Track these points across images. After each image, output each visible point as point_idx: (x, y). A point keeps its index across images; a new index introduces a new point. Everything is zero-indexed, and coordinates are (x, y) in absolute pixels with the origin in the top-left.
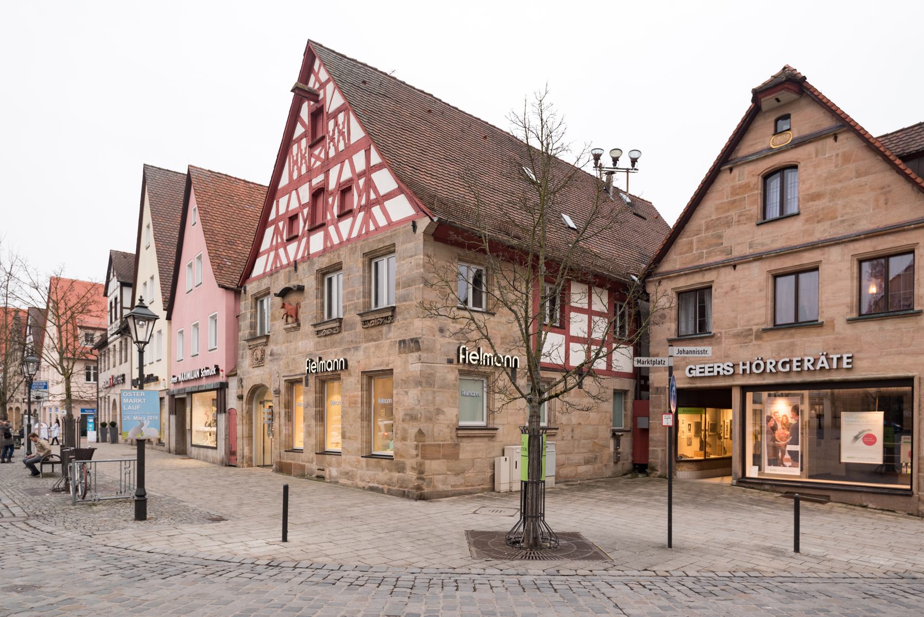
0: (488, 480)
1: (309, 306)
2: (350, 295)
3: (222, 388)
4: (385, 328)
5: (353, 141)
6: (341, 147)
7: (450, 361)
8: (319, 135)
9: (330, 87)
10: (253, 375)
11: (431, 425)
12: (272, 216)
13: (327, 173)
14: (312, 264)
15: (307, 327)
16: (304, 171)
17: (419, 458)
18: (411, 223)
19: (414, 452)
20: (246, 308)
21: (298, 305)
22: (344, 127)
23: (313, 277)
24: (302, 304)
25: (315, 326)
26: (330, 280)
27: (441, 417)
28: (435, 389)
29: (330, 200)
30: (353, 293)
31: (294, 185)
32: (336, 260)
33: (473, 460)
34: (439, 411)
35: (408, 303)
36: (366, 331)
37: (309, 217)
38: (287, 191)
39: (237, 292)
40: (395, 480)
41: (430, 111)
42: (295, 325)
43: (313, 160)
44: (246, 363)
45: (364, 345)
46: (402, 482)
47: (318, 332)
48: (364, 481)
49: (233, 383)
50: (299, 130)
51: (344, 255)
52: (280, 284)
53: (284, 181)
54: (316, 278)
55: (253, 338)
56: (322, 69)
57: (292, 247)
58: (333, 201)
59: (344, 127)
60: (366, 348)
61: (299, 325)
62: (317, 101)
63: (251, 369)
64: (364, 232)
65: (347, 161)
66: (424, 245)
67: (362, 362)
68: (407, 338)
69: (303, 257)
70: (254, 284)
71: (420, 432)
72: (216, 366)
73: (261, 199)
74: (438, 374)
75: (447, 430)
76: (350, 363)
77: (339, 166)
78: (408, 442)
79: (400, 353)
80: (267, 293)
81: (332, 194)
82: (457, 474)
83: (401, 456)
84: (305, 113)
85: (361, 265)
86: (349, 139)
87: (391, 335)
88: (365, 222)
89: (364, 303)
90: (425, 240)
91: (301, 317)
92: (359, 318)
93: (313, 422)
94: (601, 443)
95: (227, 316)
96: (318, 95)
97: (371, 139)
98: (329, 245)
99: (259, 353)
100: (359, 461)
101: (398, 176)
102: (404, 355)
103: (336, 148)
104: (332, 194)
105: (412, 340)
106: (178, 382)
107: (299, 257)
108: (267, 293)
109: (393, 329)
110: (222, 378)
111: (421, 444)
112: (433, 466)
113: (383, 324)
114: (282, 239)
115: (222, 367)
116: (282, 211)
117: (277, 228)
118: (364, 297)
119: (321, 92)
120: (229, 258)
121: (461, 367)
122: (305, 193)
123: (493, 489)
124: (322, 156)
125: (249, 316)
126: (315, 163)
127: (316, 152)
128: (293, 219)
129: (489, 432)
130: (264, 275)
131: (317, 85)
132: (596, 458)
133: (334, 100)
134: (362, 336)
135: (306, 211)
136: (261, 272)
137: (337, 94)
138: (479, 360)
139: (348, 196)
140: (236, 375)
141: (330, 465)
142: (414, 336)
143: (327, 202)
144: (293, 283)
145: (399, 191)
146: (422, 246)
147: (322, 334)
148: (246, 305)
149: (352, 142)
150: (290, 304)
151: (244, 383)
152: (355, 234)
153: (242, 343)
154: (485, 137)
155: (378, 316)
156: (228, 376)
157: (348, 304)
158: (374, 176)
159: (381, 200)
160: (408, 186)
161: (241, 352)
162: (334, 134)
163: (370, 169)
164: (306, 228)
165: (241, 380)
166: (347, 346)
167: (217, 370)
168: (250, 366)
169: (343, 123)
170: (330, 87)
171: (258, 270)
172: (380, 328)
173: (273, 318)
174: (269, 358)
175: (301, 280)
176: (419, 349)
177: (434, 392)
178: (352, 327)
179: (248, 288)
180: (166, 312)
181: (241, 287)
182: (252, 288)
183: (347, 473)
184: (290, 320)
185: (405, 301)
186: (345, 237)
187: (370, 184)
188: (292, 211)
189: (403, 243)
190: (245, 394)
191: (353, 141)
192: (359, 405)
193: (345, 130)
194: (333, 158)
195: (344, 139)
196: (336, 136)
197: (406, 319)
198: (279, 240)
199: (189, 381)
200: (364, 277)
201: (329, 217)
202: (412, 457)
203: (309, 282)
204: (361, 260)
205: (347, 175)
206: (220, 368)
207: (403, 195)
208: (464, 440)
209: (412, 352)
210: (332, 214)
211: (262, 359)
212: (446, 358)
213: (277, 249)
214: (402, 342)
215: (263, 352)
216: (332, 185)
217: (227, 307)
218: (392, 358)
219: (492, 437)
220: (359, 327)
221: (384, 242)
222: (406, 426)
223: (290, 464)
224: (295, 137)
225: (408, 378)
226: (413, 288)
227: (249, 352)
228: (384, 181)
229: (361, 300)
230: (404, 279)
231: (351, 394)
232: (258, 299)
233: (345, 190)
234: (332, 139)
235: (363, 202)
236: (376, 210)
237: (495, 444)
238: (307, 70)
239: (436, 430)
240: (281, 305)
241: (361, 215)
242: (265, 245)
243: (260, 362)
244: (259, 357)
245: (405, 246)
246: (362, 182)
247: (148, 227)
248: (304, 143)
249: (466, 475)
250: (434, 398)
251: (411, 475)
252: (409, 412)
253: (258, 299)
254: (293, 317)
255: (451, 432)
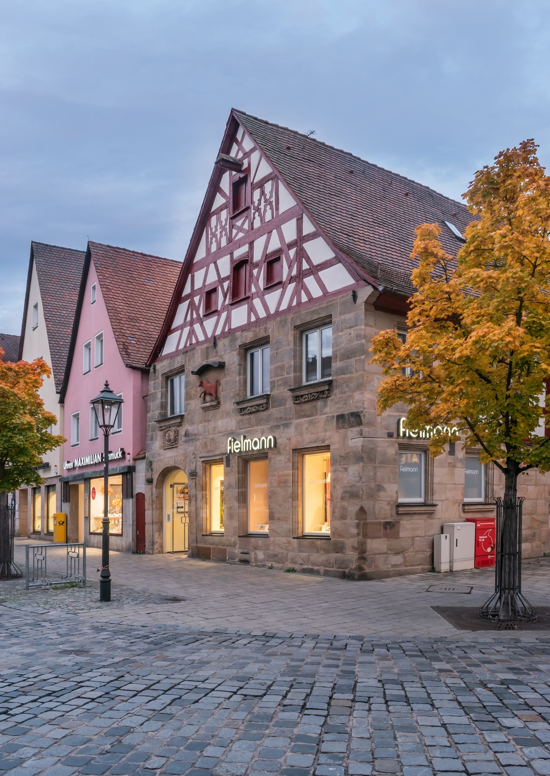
0: (428, 560)
1: (229, 384)
2: (278, 371)
3: (128, 473)
4: (319, 403)
5: (282, 210)
6: (268, 217)
7: (390, 435)
8: (243, 207)
9: (255, 156)
10: (165, 457)
11: (372, 502)
12: (187, 290)
13: (251, 244)
14: (234, 340)
15: (228, 405)
16: (224, 243)
17: (361, 537)
18: (351, 293)
19: (354, 531)
20: (155, 388)
21: (218, 383)
22: (271, 196)
23: (235, 353)
24: (223, 382)
25: (238, 403)
26: (252, 355)
27: (382, 494)
28: (377, 465)
29: (255, 271)
30: (282, 368)
31: (212, 259)
32: (262, 334)
33: (413, 538)
34: (380, 488)
35: (347, 376)
36: (298, 407)
37: (231, 291)
38: (204, 263)
39: (145, 372)
40: (332, 560)
41: (351, 172)
42: (214, 403)
43: (234, 231)
44: (156, 444)
45: (296, 422)
46: (342, 563)
47: (241, 410)
48: (295, 563)
49: (141, 467)
50: (219, 201)
51: (272, 329)
52: (198, 361)
53: (201, 254)
54: (239, 354)
55: (163, 419)
56: (247, 137)
57: (210, 323)
58: (259, 273)
59: (271, 196)
60: (298, 424)
61: (219, 403)
62: (239, 171)
63: (162, 451)
64: (294, 303)
65: (275, 232)
66: (366, 315)
67: (294, 440)
68: (346, 412)
69: (223, 332)
70: (166, 363)
71: (362, 510)
72: (122, 450)
73: (175, 275)
74: (379, 449)
75: (387, 508)
76: (279, 441)
77: (265, 237)
78: (348, 521)
79: (338, 428)
80: (181, 371)
81: (257, 265)
82: (397, 553)
83: (340, 536)
84: (226, 184)
85: (291, 339)
86: (277, 209)
87: (327, 410)
88: (297, 293)
89: (295, 377)
90: (366, 310)
91: (222, 394)
92: (289, 394)
93: (236, 504)
94: (539, 518)
95: (134, 396)
96: (241, 165)
97: (305, 206)
98: (253, 319)
99: (172, 434)
100: (289, 543)
101: (334, 245)
102: (342, 431)
103: (262, 219)
104: (257, 265)
105: (352, 414)
106: (74, 468)
107: (218, 332)
108: (181, 371)
109: (329, 403)
110: (129, 461)
111: (362, 522)
112: (375, 545)
113: (318, 399)
114: (198, 315)
115: (129, 449)
116: (198, 285)
117: (192, 304)
118: (295, 371)
119: (246, 162)
120: (133, 336)
121: (400, 441)
122: (225, 266)
123: (433, 570)
124: (246, 226)
125: (159, 395)
126: (237, 234)
127: (239, 223)
128: (210, 294)
129: (428, 508)
130: (177, 352)
131: (240, 155)
132: (534, 535)
133: (260, 168)
134: (293, 412)
135: (226, 285)
136: (173, 349)
137: (264, 162)
138: (240, 448)
139: (276, 266)
140: (144, 458)
141: (256, 548)
142: (354, 410)
143: (251, 275)
144: (213, 360)
145: (337, 260)
146: (363, 316)
147: (246, 411)
148: (155, 385)
149: (281, 212)
150: (209, 382)
151: (154, 466)
152: (284, 306)
153: (152, 423)
154: (407, 195)
155: (311, 391)
156: (135, 460)
157: (276, 379)
158: (308, 246)
159: (314, 270)
160: (345, 254)
161: (149, 434)
162: (259, 204)
163: (301, 239)
164: (227, 302)
165: (150, 464)
166: (275, 424)
167: (123, 453)
168: (161, 447)
169: (271, 192)
170: (255, 156)
171: (170, 347)
172: (314, 403)
173: (188, 397)
174: (184, 438)
175: (221, 357)
176: (360, 423)
177: (375, 468)
178: (281, 402)
179: (157, 367)
180: (59, 395)
181: (150, 366)
182: (162, 367)
183: (275, 556)
184: (208, 398)
185: (344, 374)
186: (272, 311)
187: (302, 254)
188: (210, 285)
189: (341, 314)
190: (155, 477)
191: (282, 210)
192: (290, 484)
193: (273, 199)
194: (259, 229)
195: (271, 208)
196: (262, 207)
197: (345, 393)
198: (195, 316)
199: (87, 466)
200: (295, 351)
201: (253, 290)
202: (353, 536)
203: (231, 358)
204: (291, 333)
205: (275, 244)
206: (127, 451)
207: (340, 265)
208: (405, 517)
209: (352, 427)
210: (257, 287)
211: (176, 440)
212: (386, 431)
213: (192, 324)
214: (341, 417)
215: (177, 433)
216: (257, 256)
217: (134, 388)
218: (328, 434)
219: (431, 514)
220: (290, 403)
221: (319, 314)
222: (345, 504)
223: (209, 549)
224: (213, 209)
225: (348, 454)
226: (353, 360)
227: (159, 434)
228: (319, 251)
229: (292, 375)
230: (342, 351)
231: (281, 473)
232: (169, 377)
233: (272, 261)
234: (258, 209)
235: (294, 273)
236: (309, 281)
237: (434, 521)
238: (230, 139)
239: (377, 507)
240: (198, 384)
241: (291, 287)
242: (178, 321)
243: (172, 444)
244: (172, 438)
245: (343, 317)
246: (292, 253)
247: (36, 307)
248: (224, 214)
249: (406, 555)
250: (375, 474)
251: (351, 555)
252: (349, 489)
253: (169, 377)
254: (212, 397)
255: (391, 509)
